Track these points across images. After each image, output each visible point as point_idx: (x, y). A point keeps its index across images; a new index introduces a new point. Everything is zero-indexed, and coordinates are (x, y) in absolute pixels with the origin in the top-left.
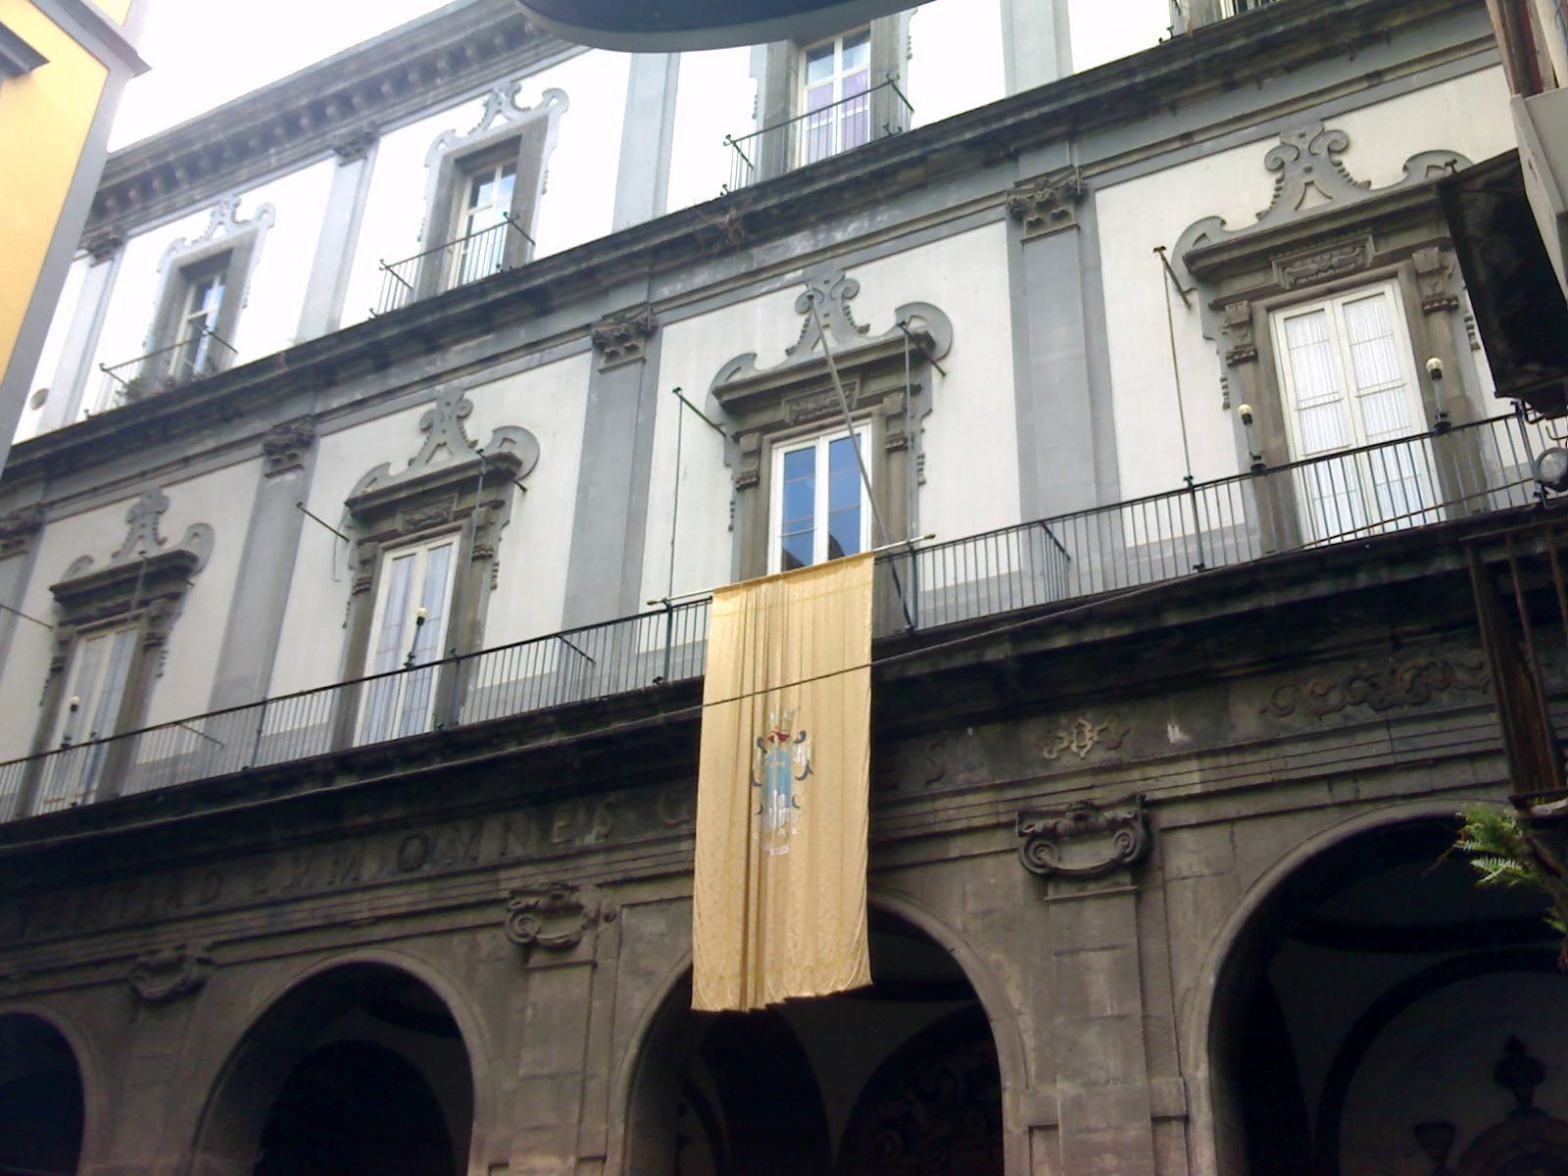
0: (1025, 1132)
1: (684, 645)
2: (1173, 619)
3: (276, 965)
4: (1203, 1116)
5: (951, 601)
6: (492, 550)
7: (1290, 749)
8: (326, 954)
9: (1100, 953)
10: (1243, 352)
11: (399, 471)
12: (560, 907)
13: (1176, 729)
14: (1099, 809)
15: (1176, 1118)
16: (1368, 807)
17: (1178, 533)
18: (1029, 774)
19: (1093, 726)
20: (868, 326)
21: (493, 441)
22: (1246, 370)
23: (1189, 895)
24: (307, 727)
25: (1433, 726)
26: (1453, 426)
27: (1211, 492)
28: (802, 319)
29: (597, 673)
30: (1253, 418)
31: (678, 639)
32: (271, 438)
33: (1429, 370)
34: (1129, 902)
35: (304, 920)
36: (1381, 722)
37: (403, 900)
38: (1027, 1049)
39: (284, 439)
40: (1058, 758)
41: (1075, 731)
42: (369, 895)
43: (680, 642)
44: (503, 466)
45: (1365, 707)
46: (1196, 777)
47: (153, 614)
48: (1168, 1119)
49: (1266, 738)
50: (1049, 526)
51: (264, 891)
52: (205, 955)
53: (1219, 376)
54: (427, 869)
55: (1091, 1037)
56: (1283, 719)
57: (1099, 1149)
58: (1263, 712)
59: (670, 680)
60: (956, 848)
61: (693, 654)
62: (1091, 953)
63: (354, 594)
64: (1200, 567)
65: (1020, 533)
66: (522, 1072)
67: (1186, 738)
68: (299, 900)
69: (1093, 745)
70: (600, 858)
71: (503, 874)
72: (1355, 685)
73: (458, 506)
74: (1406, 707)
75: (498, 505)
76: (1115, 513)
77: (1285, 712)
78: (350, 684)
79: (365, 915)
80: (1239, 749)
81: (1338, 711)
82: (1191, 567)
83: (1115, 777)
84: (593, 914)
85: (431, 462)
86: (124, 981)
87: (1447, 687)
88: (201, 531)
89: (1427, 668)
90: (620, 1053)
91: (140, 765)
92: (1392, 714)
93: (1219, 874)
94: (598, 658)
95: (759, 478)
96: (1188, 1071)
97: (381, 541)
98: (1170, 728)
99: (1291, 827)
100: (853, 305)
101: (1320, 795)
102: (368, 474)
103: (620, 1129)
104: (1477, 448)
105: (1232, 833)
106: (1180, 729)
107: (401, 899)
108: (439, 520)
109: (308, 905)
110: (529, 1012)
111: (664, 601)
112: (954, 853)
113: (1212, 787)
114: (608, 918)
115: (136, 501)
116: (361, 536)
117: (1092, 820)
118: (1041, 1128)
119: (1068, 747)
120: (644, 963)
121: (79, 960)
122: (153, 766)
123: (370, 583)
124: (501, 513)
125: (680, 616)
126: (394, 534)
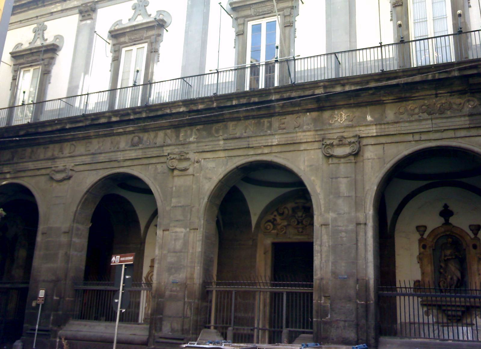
0: (320, 226)
1: (226, 82)
2: (372, 85)
3: (95, 172)
4: (370, 223)
5: (303, 75)
6: (158, 50)
7: (403, 125)
8: (109, 170)
9: (344, 179)
10: (398, 3)
11: (126, 23)
12: (183, 158)
13: (370, 117)
14: (345, 138)
15: (363, 224)
16: (423, 142)
17: (376, 58)
18: (325, 127)
19: (345, 114)
20: (122, 20)
21: (157, 15)
22: (399, 9)
23: (370, 164)
24: (102, 101)
25: (444, 120)
26: (463, 32)
27: (387, 47)
28: (34, 34)
29: (192, 90)
30: (462, 15)
31: (221, 81)
32: (81, 8)
33: (458, 14)
34: (353, 165)
35: (102, 159)
36: (430, 119)
37: (133, 155)
38: (321, 203)
39: (86, 9)
40: (334, 123)
41: (339, 116)
42: (123, 153)
43: (221, 82)
44: (161, 23)
45: (425, 114)
46: (375, 131)
47: (46, 63)
48: (360, 224)
49: (396, 121)
50: (337, 55)
51: (89, 151)
52: (72, 168)
53: (390, 10)
54: (141, 146)
55: (340, 201)
56: (401, 116)
57: (341, 231)
58: (395, 113)
59: (218, 94)
60: (303, 147)
61: (321, 71)
62: (341, 179)
63: (237, 35)
64: (382, 70)
65: (393, 46)
66: (172, 205)
67: (372, 120)
68: (101, 153)
69: (345, 120)
70: (195, 145)
71: (165, 148)
72: (423, 107)
73: (146, 35)
74: (437, 114)
75: (159, 35)
76: (354, 52)
77: (401, 113)
78: (113, 90)
79: (122, 158)
80: (388, 123)
81: (417, 115)
82: (380, 70)
83: (351, 129)
84: (193, 161)
85: (136, 20)
86: (48, 174)
87: (450, 109)
88: (59, 37)
89: (444, 104)
90: (202, 200)
91: (47, 111)
92: (433, 116)
93: (379, 158)
94: (193, 86)
95: (243, 32)
96: (367, 211)
97: (121, 45)
98: (368, 116)
99: (401, 147)
100: (147, 8)
101: (410, 138)
102: (115, 23)
103: (202, 222)
104: (467, 38)
105: (384, 148)
106: (371, 117)
107: (133, 154)
108: (140, 39)
109: (103, 155)
110: (174, 188)
111: (216, 70)
112: (302, 149)
113: (471, 126)
114: (197, 162)
115: (35, 25)
116: (115, 42)
117: (343, 141)
118: (324, 225)
119: (337, 120)
120: (208, 176)
121: (33, 168)
122: (52, 111)
123: (118, 58)
124: (160, 38)
125: (90, 96)
126: (125, 43)
